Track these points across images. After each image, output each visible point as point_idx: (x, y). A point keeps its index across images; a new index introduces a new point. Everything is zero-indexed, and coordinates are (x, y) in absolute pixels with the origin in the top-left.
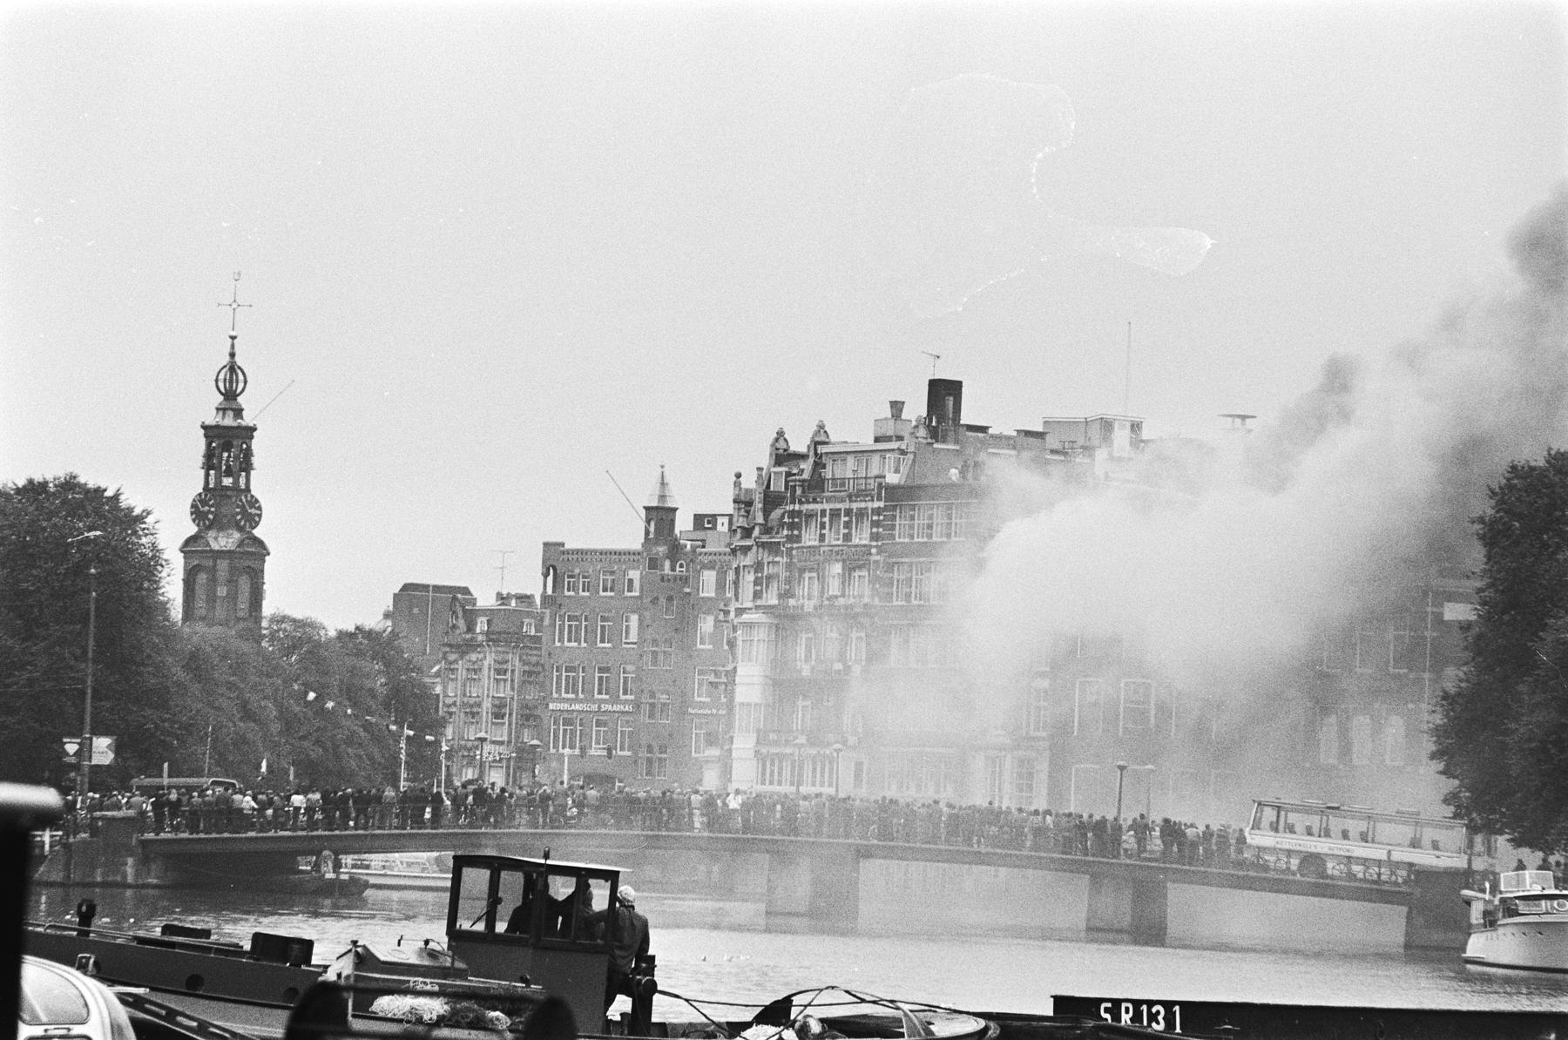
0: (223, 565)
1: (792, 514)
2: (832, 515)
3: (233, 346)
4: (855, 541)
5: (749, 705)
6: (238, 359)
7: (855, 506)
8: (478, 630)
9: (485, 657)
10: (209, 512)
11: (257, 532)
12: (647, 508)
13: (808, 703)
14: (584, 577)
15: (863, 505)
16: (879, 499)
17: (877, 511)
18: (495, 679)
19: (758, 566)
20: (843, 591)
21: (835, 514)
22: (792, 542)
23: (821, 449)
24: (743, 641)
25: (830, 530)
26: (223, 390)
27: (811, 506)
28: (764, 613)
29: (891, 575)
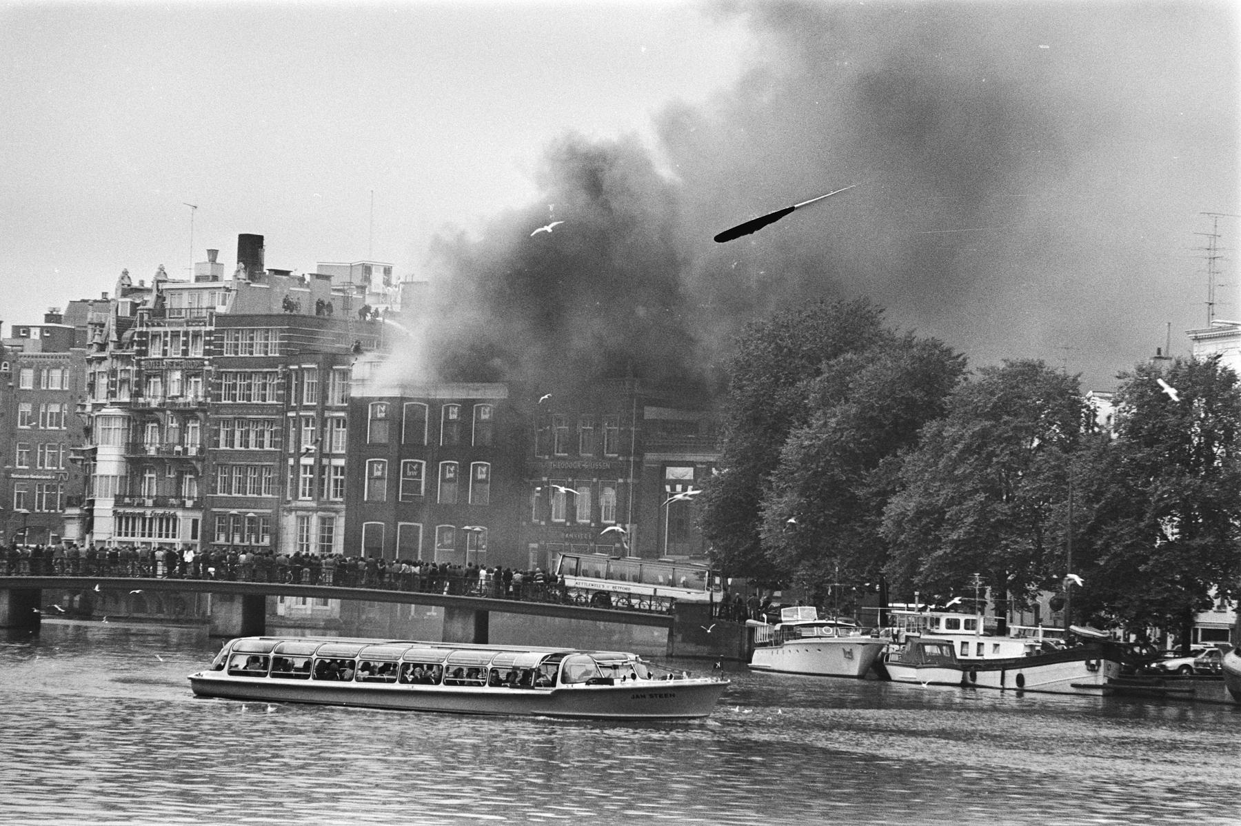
1: (141, 334)
2: (172, 336)
5: (107, 477)
7: (191, 329)
16: (211, 324)
17: (209, 333)
19: (113, 373)
20: (182, 392)
21: (175, 335)
22: (140, 355)
23: (161, 286)
24: (104, 429)
29: (220, 381)
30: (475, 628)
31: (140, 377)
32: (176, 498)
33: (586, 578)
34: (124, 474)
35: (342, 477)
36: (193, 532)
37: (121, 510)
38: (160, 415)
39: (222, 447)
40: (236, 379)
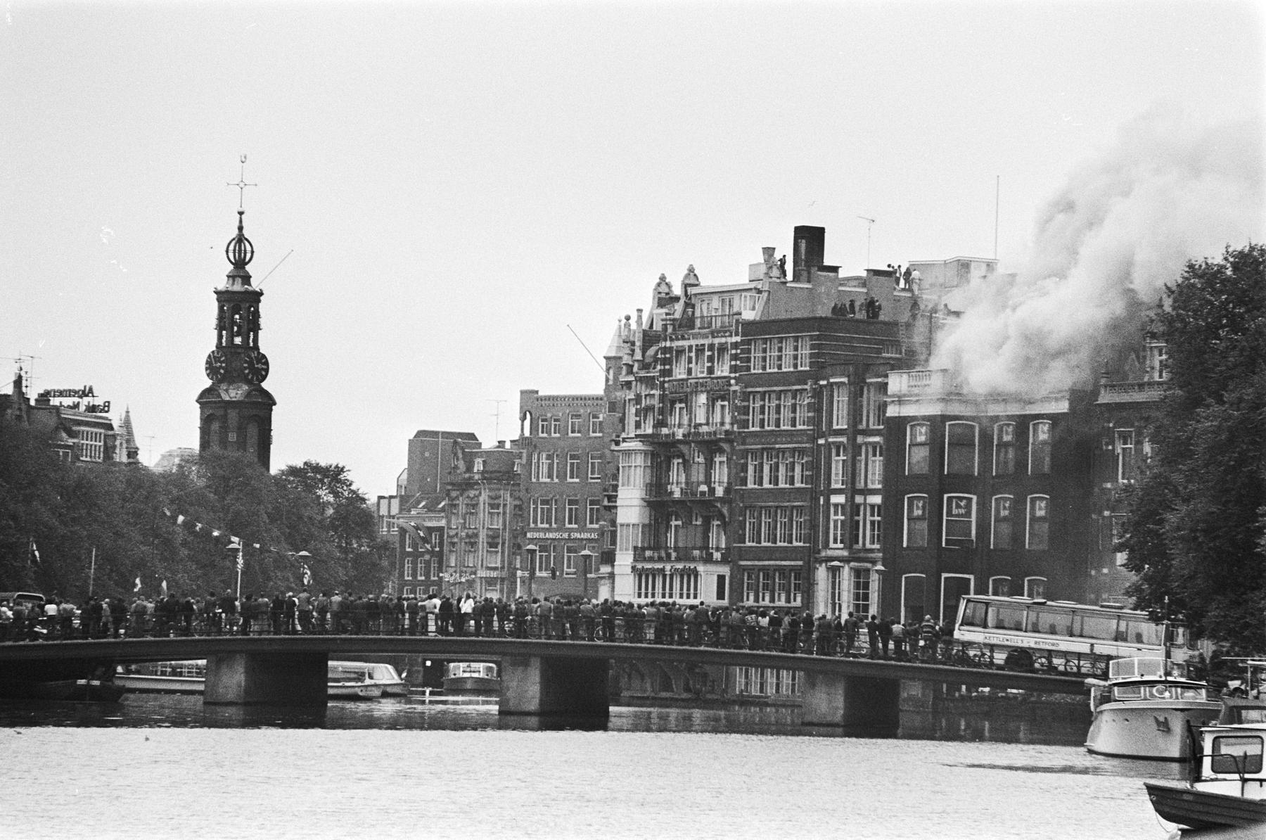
0: (233, 415)
3: (241, 221)
4: (718, 373)
5: (628, 525)
6: (245, 232)
7: (717, 341)
8: (475, 470)
9: (480, 493)
10: (221, 367)
11: (265, 385)
12: (607, 358)
13: (679, 523)
14: (555, 420)
15: (723, 340)
16: (737, 335)
17: (735, 345)
18: (489, 513)
19: (638, 399)
21: (700, 350)
23: (691, 291)
25: (697, 364)
26: (233, 261)
27: (680, 343)
28: (640, 441)
29: (746, 404)
30: (845, 701)
31: (663, 402)
32: (700, 549)
33: (1054, 637)
34: (647, 522)
35: (879, 518)
36: (718, 587)
37: (639, 566)
38: (684, 449)
39: (750, 486)
40: (764, 400)
